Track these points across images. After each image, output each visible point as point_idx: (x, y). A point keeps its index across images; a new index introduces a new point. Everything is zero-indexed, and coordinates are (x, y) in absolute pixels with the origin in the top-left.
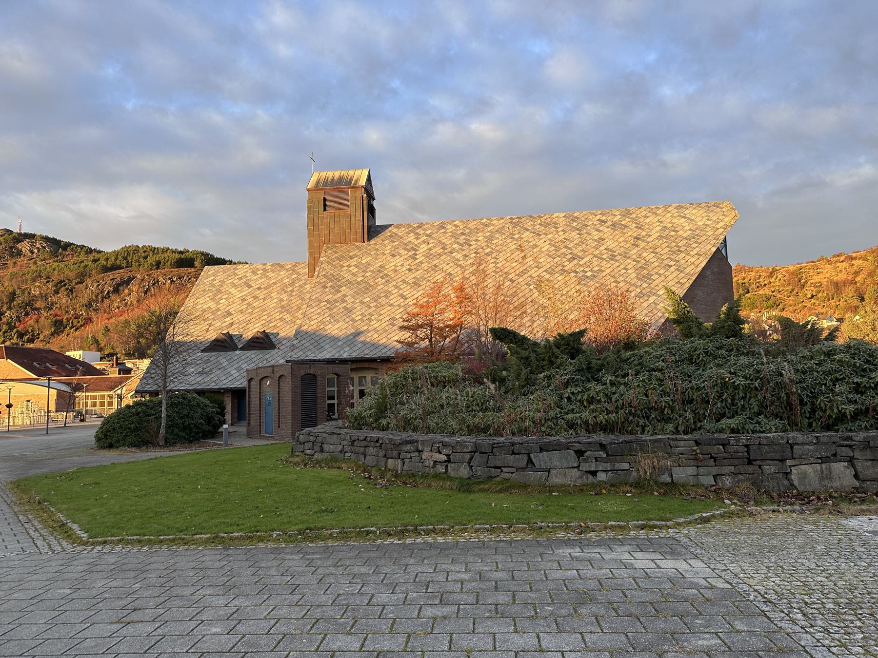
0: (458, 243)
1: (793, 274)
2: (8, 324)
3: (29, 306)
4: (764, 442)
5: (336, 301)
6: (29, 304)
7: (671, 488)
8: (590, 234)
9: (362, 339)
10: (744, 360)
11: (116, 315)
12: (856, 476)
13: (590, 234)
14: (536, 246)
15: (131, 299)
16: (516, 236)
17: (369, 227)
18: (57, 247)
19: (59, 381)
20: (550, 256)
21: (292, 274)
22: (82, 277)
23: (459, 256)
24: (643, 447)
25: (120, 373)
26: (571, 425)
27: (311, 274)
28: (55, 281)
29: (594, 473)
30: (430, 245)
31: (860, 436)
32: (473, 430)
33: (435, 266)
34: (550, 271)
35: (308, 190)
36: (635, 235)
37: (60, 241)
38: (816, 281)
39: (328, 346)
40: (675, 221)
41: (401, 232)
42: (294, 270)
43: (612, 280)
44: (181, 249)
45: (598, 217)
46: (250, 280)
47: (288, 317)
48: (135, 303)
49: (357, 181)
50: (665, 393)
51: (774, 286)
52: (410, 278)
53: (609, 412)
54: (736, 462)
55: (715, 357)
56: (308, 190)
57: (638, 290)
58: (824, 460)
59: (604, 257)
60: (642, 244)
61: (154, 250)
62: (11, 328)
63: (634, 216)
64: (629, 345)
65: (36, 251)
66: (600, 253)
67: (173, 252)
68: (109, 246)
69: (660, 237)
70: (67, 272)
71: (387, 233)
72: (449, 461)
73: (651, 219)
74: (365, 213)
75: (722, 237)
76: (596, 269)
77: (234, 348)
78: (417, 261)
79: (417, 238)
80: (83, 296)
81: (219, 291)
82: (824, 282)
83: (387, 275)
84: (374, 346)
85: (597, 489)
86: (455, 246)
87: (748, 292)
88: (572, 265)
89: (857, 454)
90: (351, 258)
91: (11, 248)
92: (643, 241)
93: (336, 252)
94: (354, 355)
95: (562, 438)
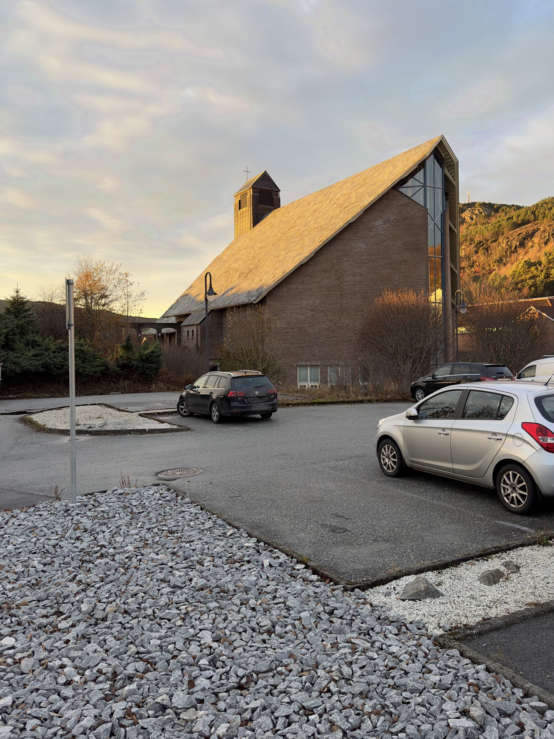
36: (237, 277)
65: (475, 217)
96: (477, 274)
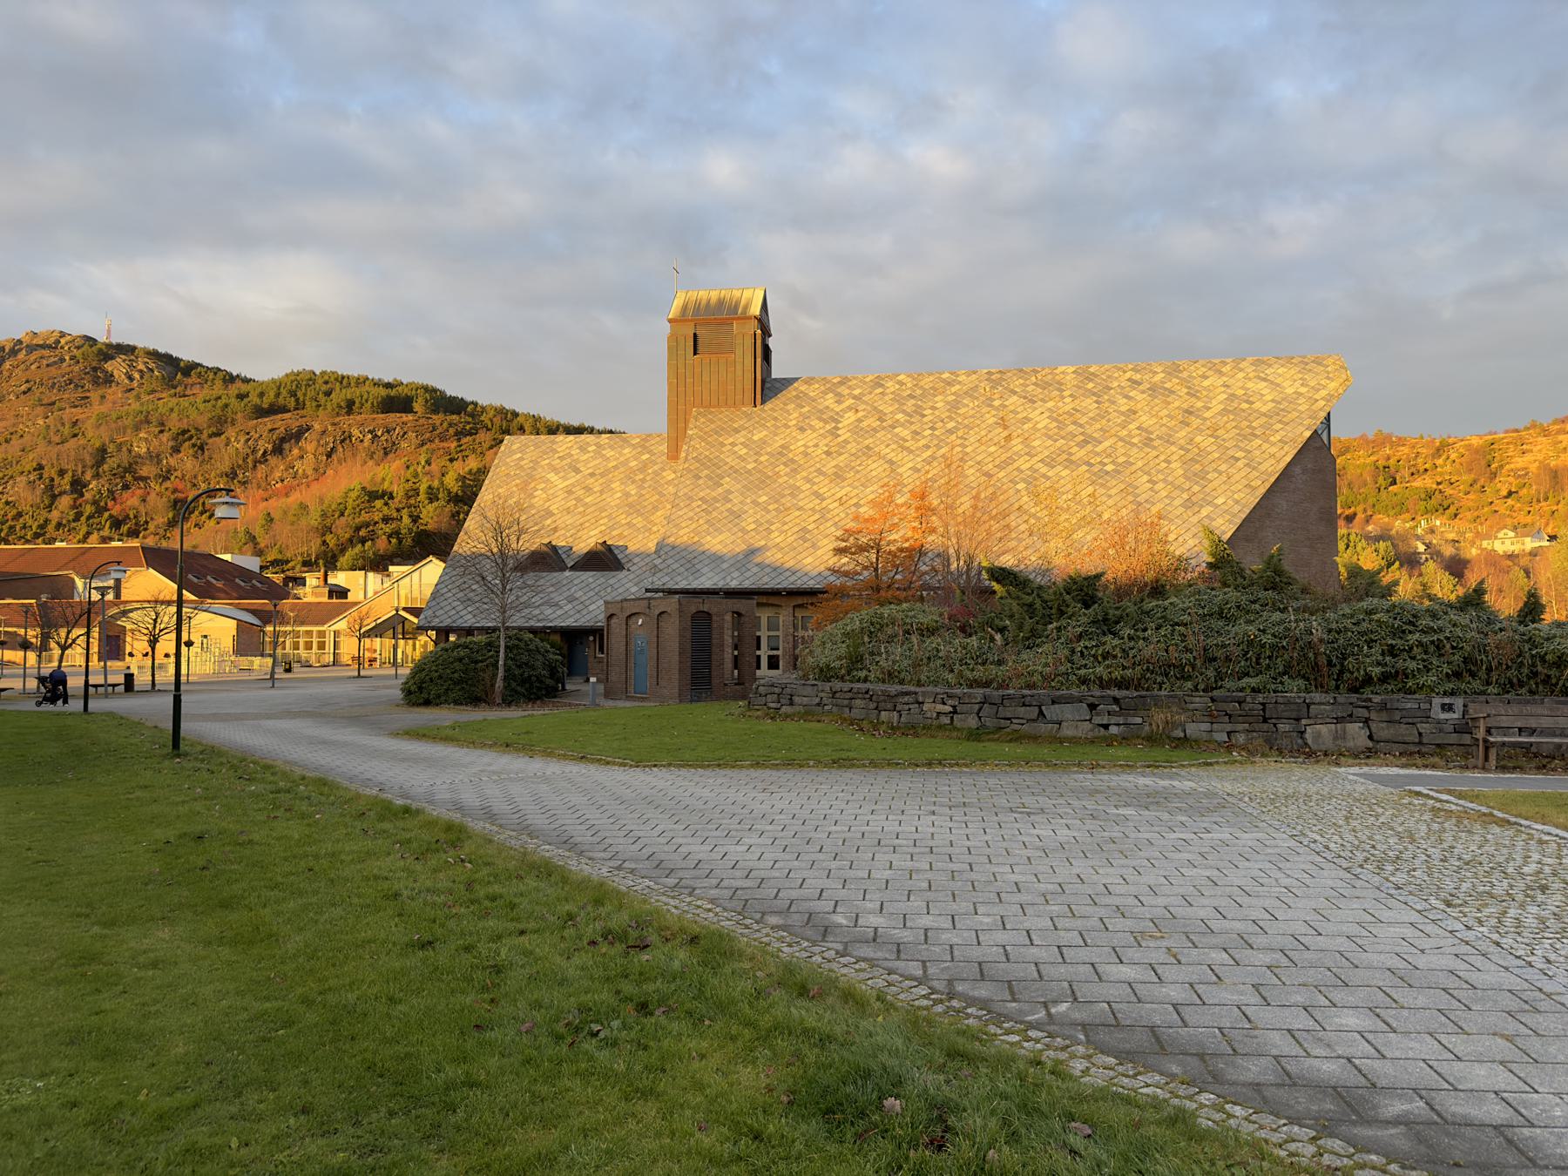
0: (904, 412)
1: (1477, 451)
2: (95, 503)
3: (129, 475)
4: (1280, 700)
5: (715, 500)
6: (129, 469)
7: (1184, 742)
8: (1113, 403)
9: (758, 560)
10: (1277, 616)
11: (277, 494)
12: (1370, 737)
13: (1113, 403)
14: (1027, 419)
15: (305, 466)
16: (997, 403)
17: (763, 382)
18: (174, 370)
19: (238, 607)
20: (1050, 437)
21: (641, 453)
22: (220, 425)
23: (905, 433)
24: (1157, 702)
25: (330, 597)
26: (1084, 681)
27: (674, 454)
28: (174, 430)
29: (1106, 727)
30: (860, 414)
31: (1377, 699)
32: (974, 683)
33: (868, 447)
34: (1050, 462)
35: (670, 321)
36: (1185, 406)
37: (178, 360)
38: (1519, 466)
39: (705, 570)
40: (1250, 385)
41: (813, 391)
42: (644, 447)
43: (1145, 478)
44: (388, 379)
45: (1128, 375)
46: (577, 461)
47: (638, 521)
48: (310, 472)
49: (746, 307)
50: (1187, 650)
51: (1441, 474)
52: (830, 466)
53: (1124, 668)
54: (1251, 719)
55: (1248, 612)
56: (670, 321)
57: (1185, 496)
58: (1339, 720)
59: (1135, 440)
60: (1196, 422)
61: (342, 380)
62: (100, 510)
63: (1185, 375)
64: (1157, 590)
65: (137, 376)
66: (1129, 435)
67: (376, 384)
68: (265, 369)
69: (1225, 412)
70: (194, 414)
71: (790, 392)
72: (955, 712)
73: (1213, 380)
74: (759, 360)
75: (1324, 414)
76: (1121, 460)
77: (563, 568)
78: (840, 439)
79: (839, 402)
80: (222, 458)
81: (531, 477)
82: (1533, 468)
83: (793, 461)
84: (776, 570)
85: (1109, 742)
86: (900, 416)
87: (1394, 483)
88: (1083, 452)
89: (1373, 716)
90: (737, 431)
91: (95, 369)
92: (1198, 417)
93: (712, 422)
94: (747, 584)
95: (1074, 692)
96: (180, 495)
